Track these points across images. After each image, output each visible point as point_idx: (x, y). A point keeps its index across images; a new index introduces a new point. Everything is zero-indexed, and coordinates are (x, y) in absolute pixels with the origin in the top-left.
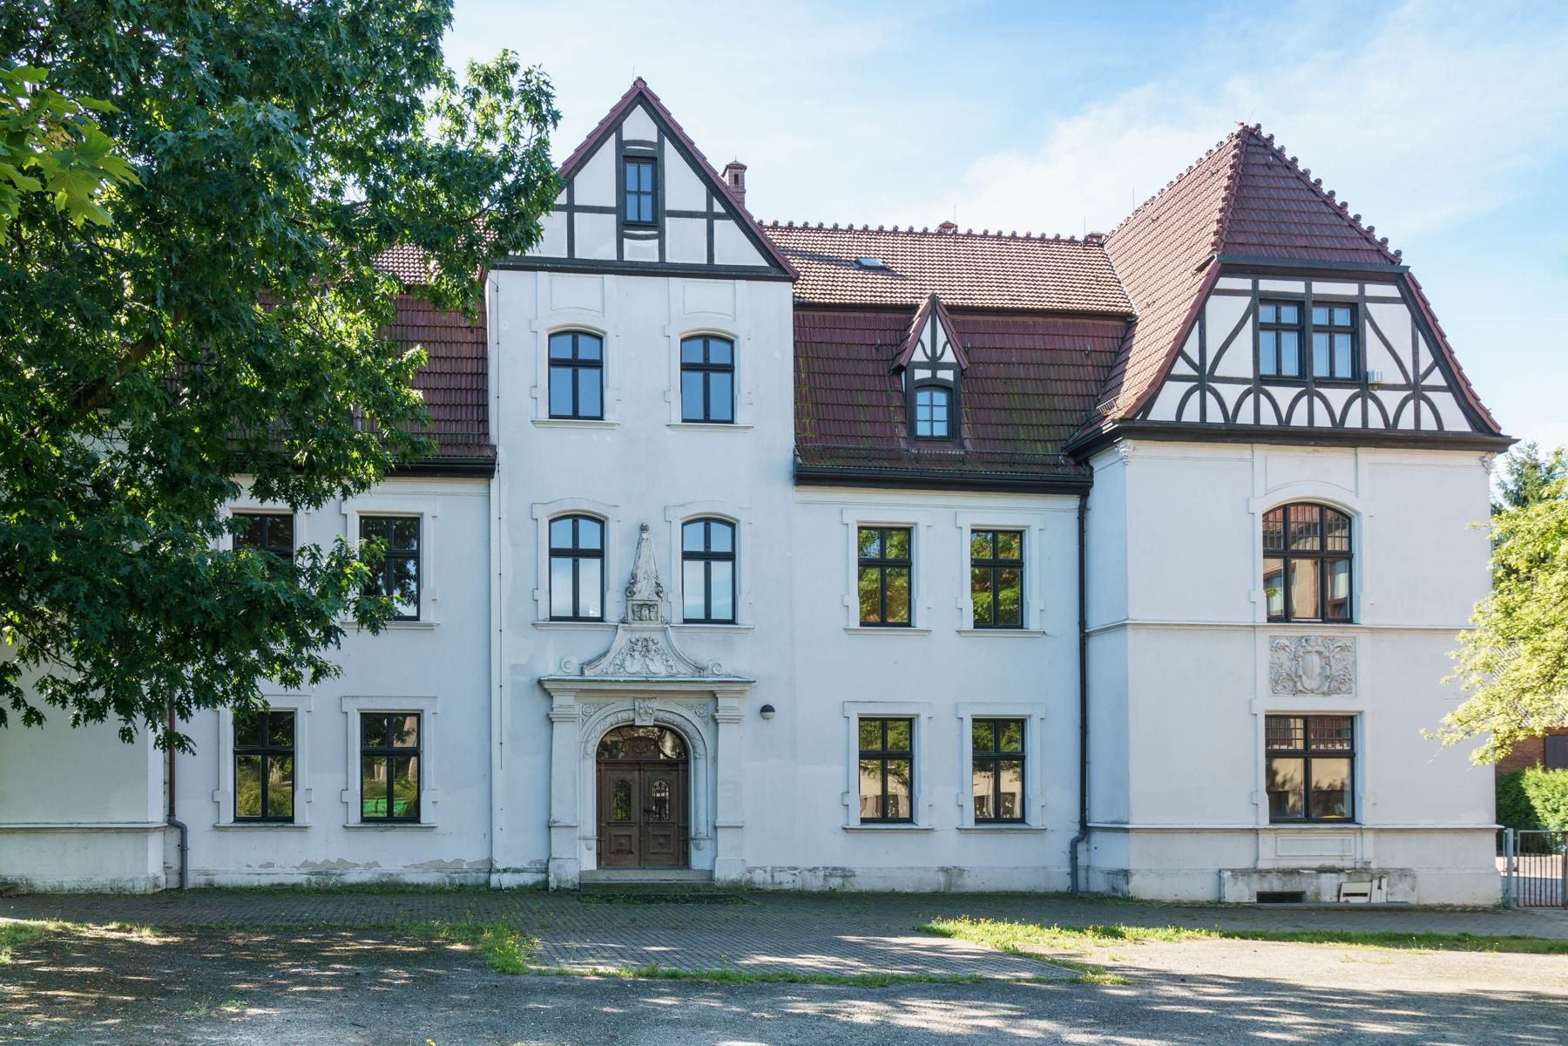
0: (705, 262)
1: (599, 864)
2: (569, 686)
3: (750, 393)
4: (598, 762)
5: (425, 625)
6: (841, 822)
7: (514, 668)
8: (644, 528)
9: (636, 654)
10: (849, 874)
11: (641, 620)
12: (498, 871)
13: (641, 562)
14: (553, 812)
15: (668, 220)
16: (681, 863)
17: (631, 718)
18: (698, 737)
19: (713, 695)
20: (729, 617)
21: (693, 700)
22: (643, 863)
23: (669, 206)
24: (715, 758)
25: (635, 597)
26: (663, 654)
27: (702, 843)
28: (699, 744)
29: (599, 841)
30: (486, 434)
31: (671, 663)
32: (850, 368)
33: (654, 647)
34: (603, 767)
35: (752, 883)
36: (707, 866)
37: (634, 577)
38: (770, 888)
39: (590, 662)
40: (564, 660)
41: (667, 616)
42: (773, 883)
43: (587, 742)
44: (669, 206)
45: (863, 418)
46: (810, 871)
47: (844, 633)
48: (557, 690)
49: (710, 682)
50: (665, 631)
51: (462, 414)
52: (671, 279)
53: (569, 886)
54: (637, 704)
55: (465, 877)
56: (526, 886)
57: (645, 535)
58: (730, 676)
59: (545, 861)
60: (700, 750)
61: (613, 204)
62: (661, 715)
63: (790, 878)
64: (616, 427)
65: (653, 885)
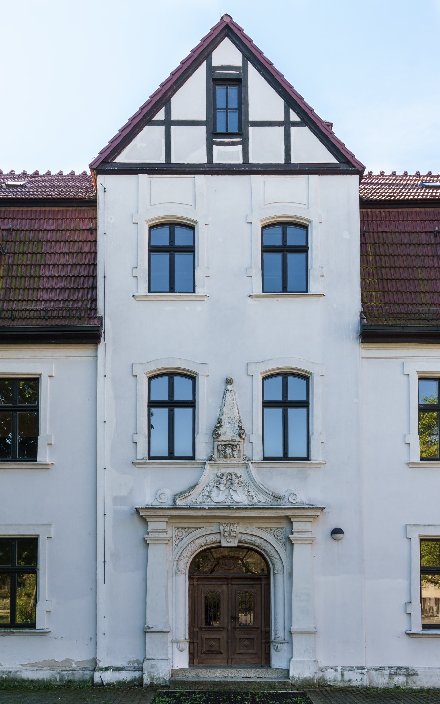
0: (283, 162)
1: (191, 663)
2: (161, 513)
3: (321, 267)
4: (190, 578)
5: (42, 465)
6: (405, 628)
7: (116, 499)
8: (229, 381)
9: (222, 487)
10: (412, 673)
11: (226, 457)
12: (101, 669)
13: (225, 409)
14: (148, 620)
15: (251, 129)
16: (263, 662)
17: (218, 540)
18: (276, 555)
19: (288, 520)
20: (305, 455)
21: (273, 525)
22: (230, 661)
23: (252, 117)
24: (291, 574)
25: (220, 439)
26: (246, 486)
27: (280, 646)
28: (277, 561)
29: (191, 644)
30: (95, 310)
31: (252, 493)
32: (412, 250)
33: (237, 481)
34: (196, 582)
35: (324, 680)
36: (284, 666)
37: (219, 422)
38: (340, 684)
39: (181, 494)
40: (159, 492)
41: (248, 453)
42: (343, 680)
43: (179, 560)
44: (252, 117)
45: (422, 289)
46: (376, 670)
47: (406, 466)
48: (151, 517)
49: (284, 509)
50: (246, 466)
51: (80, 295)
52: (253, 176)
53: (161, 682)
54: (222, 528)
55: (73, 674)
56: (125, 682)
57: (229, 387)
58: (304, 503)
59: (142, 661)
60: (278, 566)
61: (203, 117)
62: (244, 537)
63: (359, 677)
64: (205, 299)
65: (234, 683)
